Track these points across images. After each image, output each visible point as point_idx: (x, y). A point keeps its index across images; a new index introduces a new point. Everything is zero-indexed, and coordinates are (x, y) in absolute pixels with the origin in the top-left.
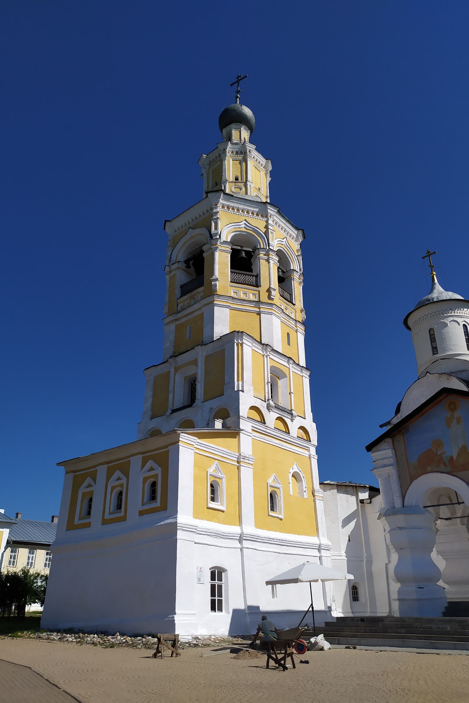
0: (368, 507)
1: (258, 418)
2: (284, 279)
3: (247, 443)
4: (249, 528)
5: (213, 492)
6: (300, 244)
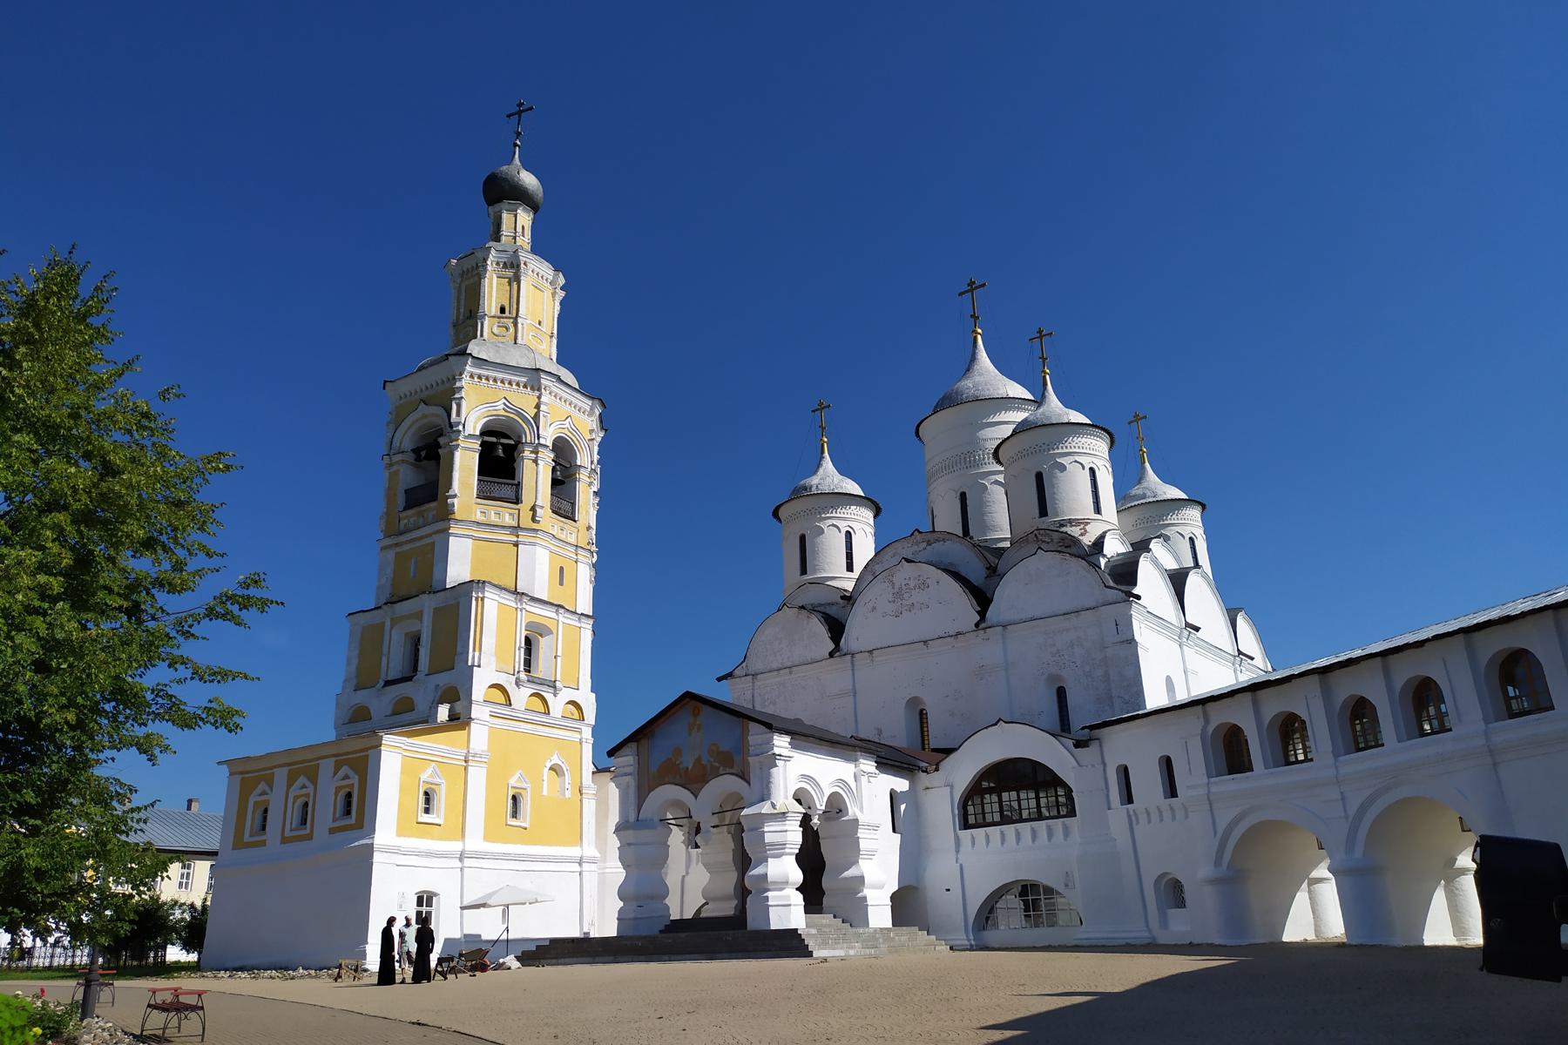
1: (502, 699)
2: (563, 481)
3: (479, 734)
4: (475, 842)
5: (428, 801)
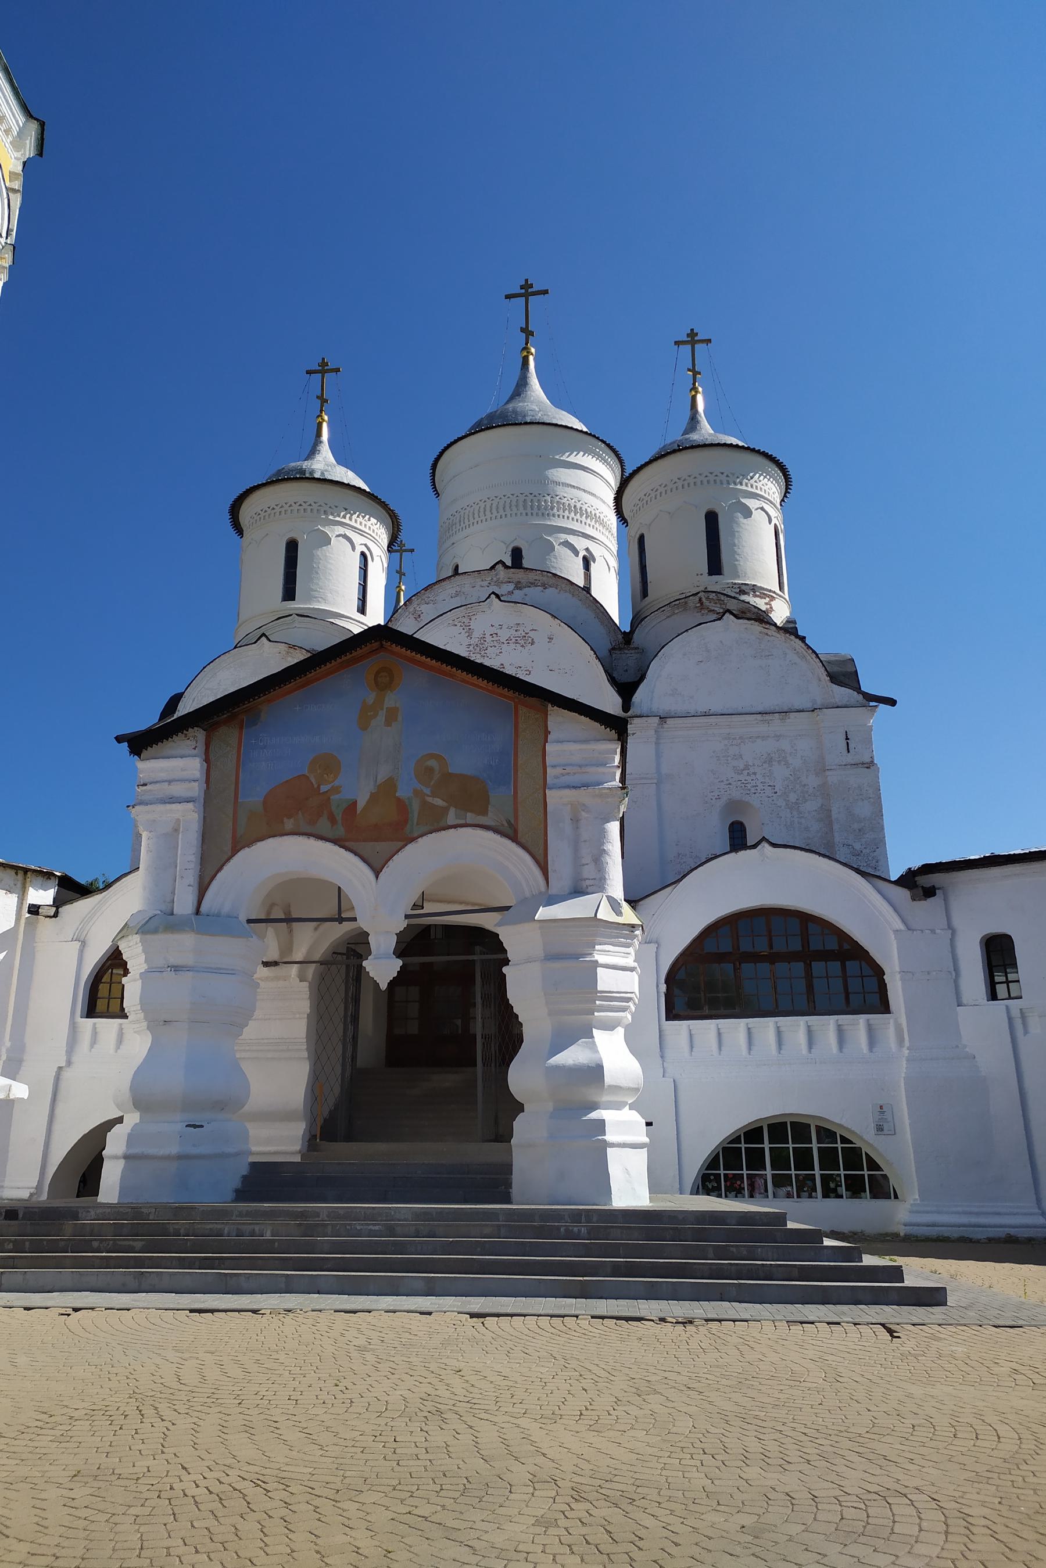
0: (45, 926)
6: (24, 163)
